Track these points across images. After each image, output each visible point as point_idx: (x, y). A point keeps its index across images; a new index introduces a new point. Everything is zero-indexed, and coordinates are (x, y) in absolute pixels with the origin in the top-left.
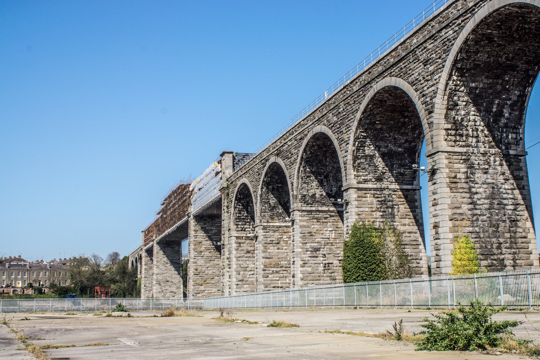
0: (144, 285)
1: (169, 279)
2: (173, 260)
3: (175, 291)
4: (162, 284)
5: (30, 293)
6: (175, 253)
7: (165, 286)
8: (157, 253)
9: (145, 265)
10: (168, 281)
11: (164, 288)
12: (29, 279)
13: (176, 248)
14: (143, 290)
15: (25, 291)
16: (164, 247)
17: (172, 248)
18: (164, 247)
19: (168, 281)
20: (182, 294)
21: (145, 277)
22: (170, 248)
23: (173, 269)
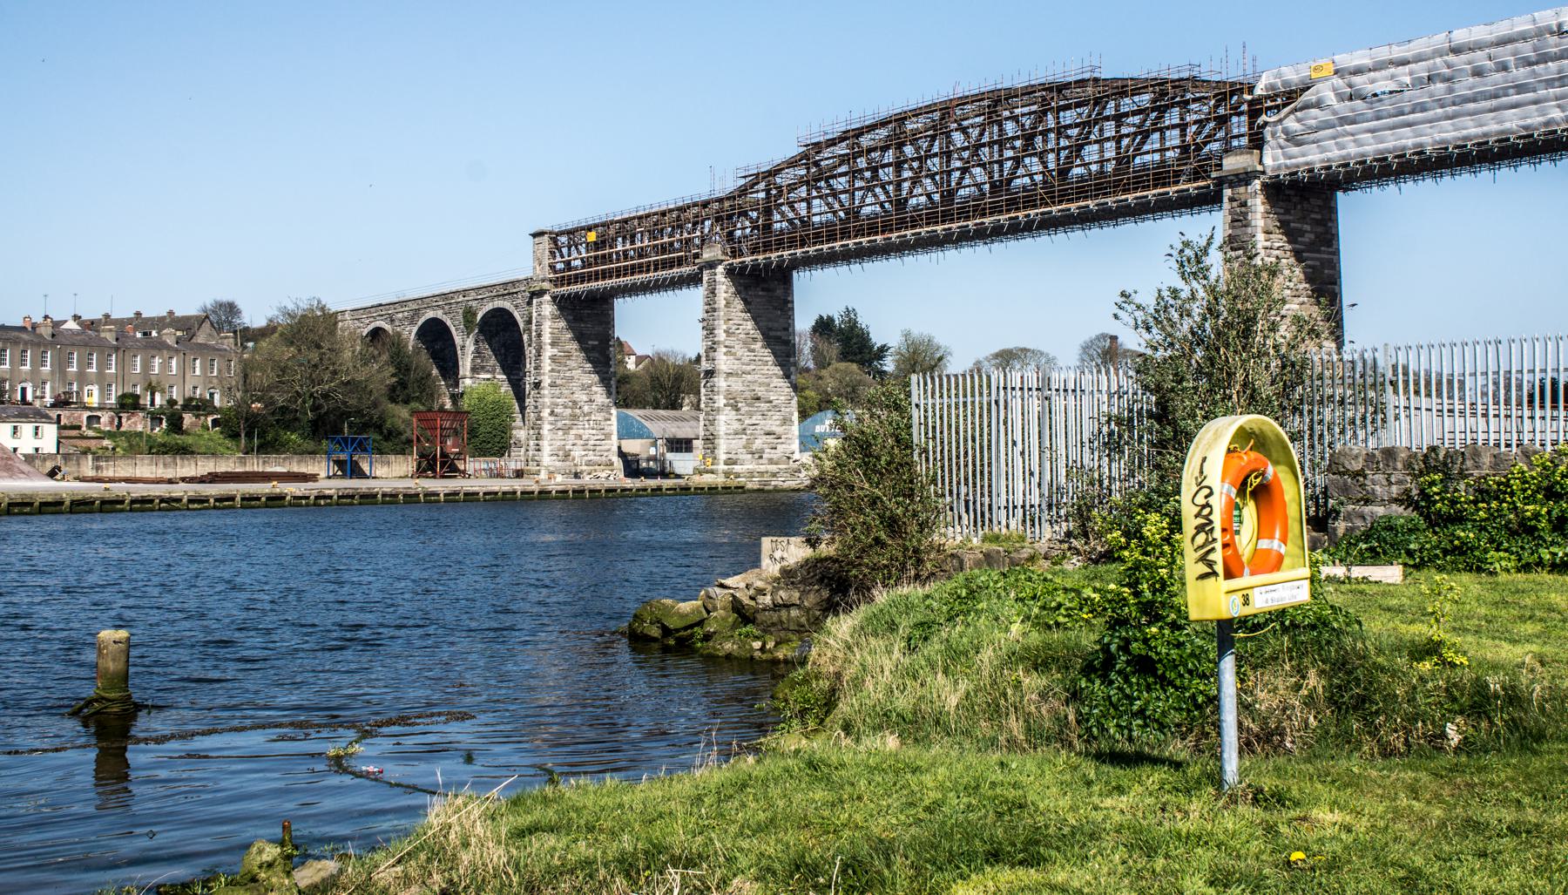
0: (548, 411)
1: (761, 391)
2: (770, 329)
3: (779, 430)
4: (744, 409)
5: (140, 428)
6: (775, 308)
7: (750, 415)
8: (728, 305)
9: (553, 344)
10: (758, 399)
11: (747, 422)
12: (120, 379)
13: (779, 292)
14: (549, 427)
15: (124, 420)
16: (747, 288)
17: (768, 290)
18: (747, 288)
19: (758, 399)
20: (797, 441)
21: (553, 385)
22: (763, 290)
23: (771, 359)
